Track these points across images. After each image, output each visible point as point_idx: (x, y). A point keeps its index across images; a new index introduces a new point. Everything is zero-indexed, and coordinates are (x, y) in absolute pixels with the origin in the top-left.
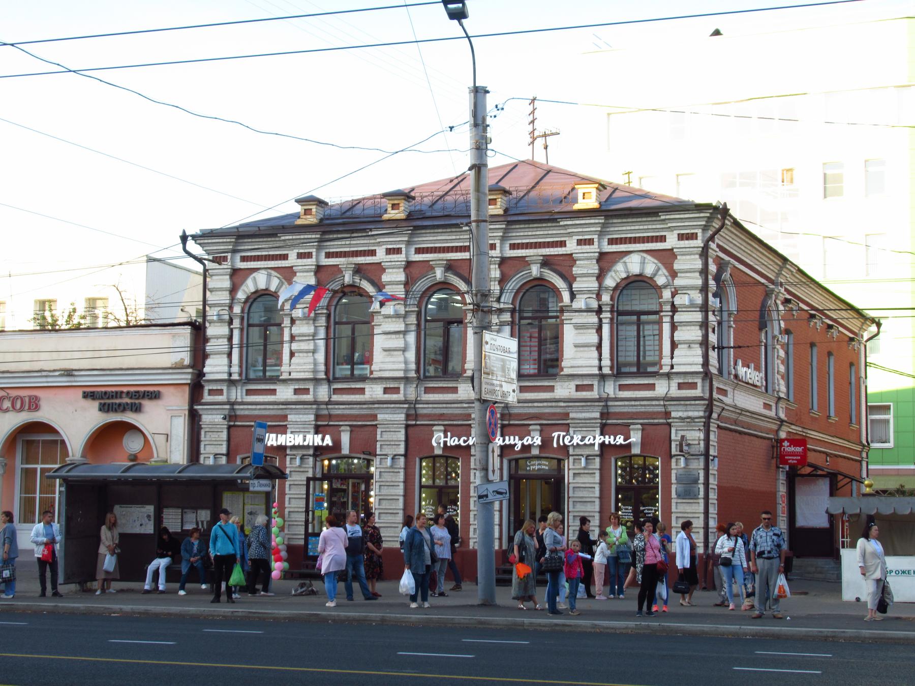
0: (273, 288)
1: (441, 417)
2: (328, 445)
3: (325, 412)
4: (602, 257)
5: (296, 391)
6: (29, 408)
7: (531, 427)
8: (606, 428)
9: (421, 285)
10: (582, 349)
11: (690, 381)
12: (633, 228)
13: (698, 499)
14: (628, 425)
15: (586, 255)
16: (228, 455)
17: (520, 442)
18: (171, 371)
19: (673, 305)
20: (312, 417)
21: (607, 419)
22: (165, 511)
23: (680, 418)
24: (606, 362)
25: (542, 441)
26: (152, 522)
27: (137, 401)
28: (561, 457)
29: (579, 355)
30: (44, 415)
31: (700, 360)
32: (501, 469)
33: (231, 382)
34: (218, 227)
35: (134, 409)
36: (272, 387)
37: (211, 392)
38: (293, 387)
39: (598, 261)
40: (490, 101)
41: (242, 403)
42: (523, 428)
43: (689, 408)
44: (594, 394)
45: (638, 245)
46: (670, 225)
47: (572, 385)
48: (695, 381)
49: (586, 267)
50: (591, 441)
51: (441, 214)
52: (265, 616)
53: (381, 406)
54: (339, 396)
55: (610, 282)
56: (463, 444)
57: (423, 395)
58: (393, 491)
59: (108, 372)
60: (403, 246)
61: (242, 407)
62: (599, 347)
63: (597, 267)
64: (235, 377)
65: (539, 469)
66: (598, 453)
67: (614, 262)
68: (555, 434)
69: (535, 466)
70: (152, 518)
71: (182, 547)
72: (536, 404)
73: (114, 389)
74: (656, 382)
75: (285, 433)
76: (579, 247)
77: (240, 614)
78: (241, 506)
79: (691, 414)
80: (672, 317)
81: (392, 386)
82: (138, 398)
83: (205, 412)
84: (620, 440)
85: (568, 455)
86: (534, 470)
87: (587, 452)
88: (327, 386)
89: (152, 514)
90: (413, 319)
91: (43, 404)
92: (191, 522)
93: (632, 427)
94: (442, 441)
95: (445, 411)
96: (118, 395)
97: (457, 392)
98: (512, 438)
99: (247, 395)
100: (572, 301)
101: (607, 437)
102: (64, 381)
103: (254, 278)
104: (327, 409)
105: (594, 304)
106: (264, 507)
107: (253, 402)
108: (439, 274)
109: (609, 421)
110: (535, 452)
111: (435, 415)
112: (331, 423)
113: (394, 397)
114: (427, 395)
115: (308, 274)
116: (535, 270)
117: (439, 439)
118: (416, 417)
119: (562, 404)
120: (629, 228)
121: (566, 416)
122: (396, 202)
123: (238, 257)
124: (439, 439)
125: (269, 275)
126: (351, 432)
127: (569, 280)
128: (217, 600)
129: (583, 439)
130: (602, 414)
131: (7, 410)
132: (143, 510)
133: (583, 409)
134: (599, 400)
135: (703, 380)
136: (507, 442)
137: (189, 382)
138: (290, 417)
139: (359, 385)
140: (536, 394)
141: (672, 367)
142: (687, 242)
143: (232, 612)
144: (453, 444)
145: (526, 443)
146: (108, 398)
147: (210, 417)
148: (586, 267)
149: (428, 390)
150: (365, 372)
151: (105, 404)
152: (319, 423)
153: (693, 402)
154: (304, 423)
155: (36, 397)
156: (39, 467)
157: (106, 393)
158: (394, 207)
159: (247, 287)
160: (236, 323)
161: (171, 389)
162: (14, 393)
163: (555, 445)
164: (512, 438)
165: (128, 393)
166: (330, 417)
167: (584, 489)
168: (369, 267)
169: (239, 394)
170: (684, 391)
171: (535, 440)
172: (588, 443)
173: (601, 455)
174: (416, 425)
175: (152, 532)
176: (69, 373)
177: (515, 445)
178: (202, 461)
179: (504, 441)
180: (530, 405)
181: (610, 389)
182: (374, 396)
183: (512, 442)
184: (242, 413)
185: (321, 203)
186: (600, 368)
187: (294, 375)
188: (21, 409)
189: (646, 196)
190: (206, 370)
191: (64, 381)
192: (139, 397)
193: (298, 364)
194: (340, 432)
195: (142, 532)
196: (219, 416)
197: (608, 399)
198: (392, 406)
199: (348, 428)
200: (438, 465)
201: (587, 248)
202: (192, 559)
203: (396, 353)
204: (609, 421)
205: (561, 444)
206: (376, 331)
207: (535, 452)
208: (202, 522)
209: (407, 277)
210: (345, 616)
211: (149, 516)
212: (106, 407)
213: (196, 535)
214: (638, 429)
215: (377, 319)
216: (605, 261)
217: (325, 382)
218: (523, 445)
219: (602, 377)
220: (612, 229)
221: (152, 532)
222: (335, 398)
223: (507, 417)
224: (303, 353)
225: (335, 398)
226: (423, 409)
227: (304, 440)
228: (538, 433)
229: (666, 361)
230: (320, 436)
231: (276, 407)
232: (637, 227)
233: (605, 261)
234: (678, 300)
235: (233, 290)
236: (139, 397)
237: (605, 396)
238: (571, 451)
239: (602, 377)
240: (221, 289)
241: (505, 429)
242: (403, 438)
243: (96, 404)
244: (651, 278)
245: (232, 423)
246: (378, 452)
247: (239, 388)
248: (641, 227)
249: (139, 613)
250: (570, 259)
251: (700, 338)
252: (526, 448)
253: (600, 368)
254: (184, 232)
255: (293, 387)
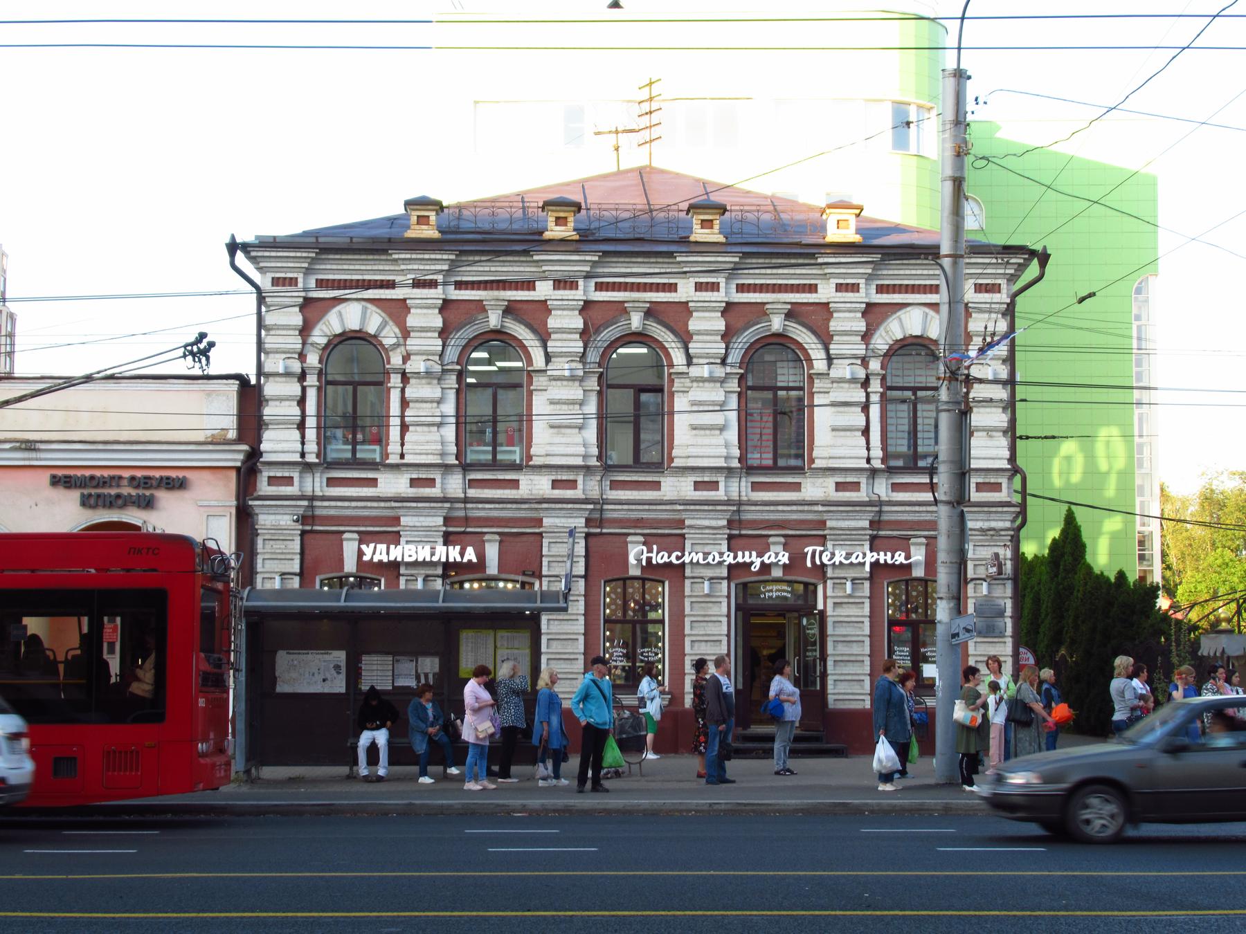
0: (371, 329)
1: (638, 523)
2: (470, 561)
3: (461, 514)
4: (870, 311)
5: (414, 482)
7: (771, 540)
8: (877, 542)
9: (609, 334)
10: (842, 433)
11: (992, 481)
12: (914, 272)
13: (1004, 636)
14: (908, 538)
15: (848, 305)
17: (759, 560)
18: (211, 447)
20: (440, 521)
21: (879, 530)
23: (981, 530)
24: (877, 452)
25: (789, 559)
26: (343, 676)
27: (148, 493)
28: (812, 581)
31: (1007, 454)
32: (729, 597)
33: (307, 467)
35: (144, 504)
36: (370, 475)
37: (272, 481)
38: (409, 476)
39: (864, 314)
41: (323, 498)
42: (763, 540)
43: (993, 516)
44: (862, 495)
45: (918, 296)
46: (403, 267)
47: (830, 482)
48: (999, 481)
49: (847, 322)
50: (860, 559)
51: (631, 236)
52: (763, 808)
53: (553, 506)
54: (479, 491)
56: (675, 562)
57: (609, 492)
59: (101, 447)
61: (326, 504)
62: (866, 432)
63: (301, 317)
65: (777, 597)
66: (298, 571)
67: (884, 317)
68: (809, 550)
70: (344, 670)
71: (410, 709)
72: (780, 508)
74: (662, 479)
75: (397, 543)
76: (839, 294)
77: (723, 807)
79: (993, 524)
80: (403, 391)
81: (564, 478)
82: (150, 487)
83: (265, 510)
84: (900, 558)
85: (824, 579)
86: (770, 598)
87: (709, 573)
88: (461, 476)
89: (343, 664)
90: (593, 383)
92: (407, 676)
93: (913, 540)
94: (644, 557)
95: (645, 515)
96: (115, 481)
97: (517, 487)
98: (747, 553)
99: (328, 486)
100: (830, 366)
101: (882, 553)
102: (18, 458)
103: (340, 314)
104: (465, 508)
105: (296, 367)
106: (528, 651)
108: (636, 321)
109: (882, 533)
110: (777, 573)
111: (628, 520)
112: (469, 530)
114: (614, 492)
115: (430, 311)
116: (777, 323)
117: (636, 553)
118: (601, 522)
119: (820, 508)
120: (908, 272)
121: (822, 524)
122: (562, 215)
123: (592, 283)
124: (636, 553)
126: (501, 542)
127: (825, 339)
128: (581, 790)
129: (849, 555)
132: (327, 657)
133: (418, 513)
134: (870, 504)
136: (740, 559)
137: (239, 464)
138: (403, 520)
139: (370, 475)
140: (775, 494)
141: (402, 456)
142: (986, 295)
143: (710, 805)
144: (661, 562)
145: (767, 561)
146: (97, 486)
147: (272, 517)
148: (847, 322)
149: (615, 485)
150: (512, 457)
151: (90, 495)
152: (451, 529)
153: (1000, 509)
154: (428, 529)
157: (92, 478)
158: (560, 221)
159: (329, 325)
160: (312, 380)
161: (206, 475)
163: (809, 564)
164: (747, 553)
165: (133, 478)
166: (467, 520)
168: (525, 306)
169: (317, 485)
170: (985, 494)
171: (780, 557)
172: (855, 561)
173: (871, 578)
174: (601, 534)
175: (343, 690)
176: (29, 446)
177: (752, 563)
178: (259, 586)
179: (735, 558)
180: (772, 508)
181: (882, 489)
182: (534, 492)
183: (747, 560)
184: (324, 512)
185: (439, 207)
189: (898, 229)
190: (263, 447)
191: (18, 458)
193: (416, 443)
194: (484, 542)
195: (326, 691)
196: (287, 517)
197: (881, 503)
198: (570, 506)
199: (356, 536)
200: (630, 590)
201: (850, 296)
202: (430, 730)
203: (568, 431)
204: (882, 533)
205: (818, 562)
206: (818, 400)
207: (777, 573)
208: (426, 675)
209: (585, 323)
210: (889, 805)
211: (337, 668)
212: (92, 501)
214: (920, 544)
216: (874, 314)
217: (460, 469)
218: (763, 563)
219: (873, 473)
220: (885, 272)
221: (343, 690)
222: (472, 493)
223: (736, 525)
224: (424, 426)
225: (472, 493)
226: (612, 512)
227: (433, 554)
228: (781, 547)
229: (394, 447)
230: (458, 548)
231: (382, 504)
232: (919, 272)
233: (874, 314)
235: (305, 331)
237: (875, 498)
238: (830, 573)
239: (873, 473)
242: (297, 548)
243: (75, 495)
244: (375, 336)
245: (308, 528)
246: (545, 572)
247: (317, 475)
248: (925, 272)
249: (555, 811)
250: (684, 309)
251: (1006, 425)
252: (765, 568)
253: (303, 455)
254: (233, 237)
255: (409, 476)
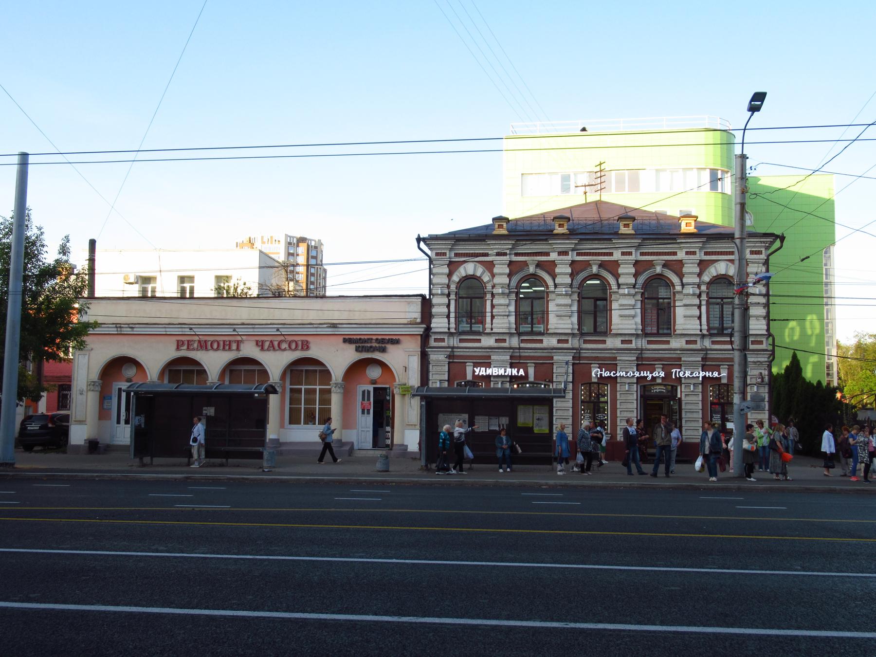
0: (478, 274)
1: (596, 358)
6: (302, 348)
16: (448, 381)
19: (492, 294)
20: (508, 357)
22: (476, 417)
24: (705, 327)
29: (688, 322)
30: (314, 352)
31: (765, 327)
33: (451, 334)
34: (447, 232)
36: (478, 337)
37: (436, 340)
40: (749, 163)
41: (458, 348)
44: (698, 346)
49: (690, 269)
55: (456, 278)
58: (629, 406)
60: (697, 250)
64: (453, 330)
69: (657, 389)
73: (366, 337)
78: (531, 414)
79: (759, 359)
84: (716, 374)
87: (694, 381)
89: (467, 420)
90: (575, 297)
91: (312, 345)
95: (599, 355)
96: (365, 341)
102: (330, 331)
106: (547, 415)
107: (467, 347)
108: (595, 269)
113: (565, 346)
116: (659, 269)
118: (579, 358)
121: (680, 359)
125: (475, 266)
127: (681, 276)
130: (702, 358)
131: (285, 350)
134: (702, 350)
135: (767, 339)
139: (478, 337)
149: (585, 342)
154: (503, 361)
155: (307, 342)
156: (303, 387)
160: (453, 297)
162: (290, 338)
165: (377, 339)
166: (520, 357)
167: (692, 402)
176: (334, 326)
181: (707, 343)
185: (507, 220)
186: (449, 329)
187: (495, 330)
188: (296, 349)
190: (432, 325)
191: (330, 331)
192: (385, 343)
197: (707, 350)
201: (692, 257)
207: (659, 381)
213: (503, 433)
215: (551, 296)
216: (703, 265)
222: (522, 345)
224: (501, 316)
225: (522, 345)
229: (488, 325)
233: (703, 265)
234: (495, 291)
236: (385, 343)
238: (683, 381)
239: (703, 336)
240: (442, 274)
241: (639, 367)
246: (554, 380)
252: (654, 378)
253: (449, 329)
